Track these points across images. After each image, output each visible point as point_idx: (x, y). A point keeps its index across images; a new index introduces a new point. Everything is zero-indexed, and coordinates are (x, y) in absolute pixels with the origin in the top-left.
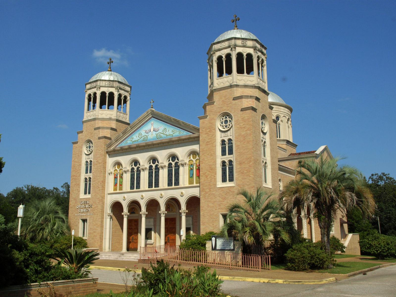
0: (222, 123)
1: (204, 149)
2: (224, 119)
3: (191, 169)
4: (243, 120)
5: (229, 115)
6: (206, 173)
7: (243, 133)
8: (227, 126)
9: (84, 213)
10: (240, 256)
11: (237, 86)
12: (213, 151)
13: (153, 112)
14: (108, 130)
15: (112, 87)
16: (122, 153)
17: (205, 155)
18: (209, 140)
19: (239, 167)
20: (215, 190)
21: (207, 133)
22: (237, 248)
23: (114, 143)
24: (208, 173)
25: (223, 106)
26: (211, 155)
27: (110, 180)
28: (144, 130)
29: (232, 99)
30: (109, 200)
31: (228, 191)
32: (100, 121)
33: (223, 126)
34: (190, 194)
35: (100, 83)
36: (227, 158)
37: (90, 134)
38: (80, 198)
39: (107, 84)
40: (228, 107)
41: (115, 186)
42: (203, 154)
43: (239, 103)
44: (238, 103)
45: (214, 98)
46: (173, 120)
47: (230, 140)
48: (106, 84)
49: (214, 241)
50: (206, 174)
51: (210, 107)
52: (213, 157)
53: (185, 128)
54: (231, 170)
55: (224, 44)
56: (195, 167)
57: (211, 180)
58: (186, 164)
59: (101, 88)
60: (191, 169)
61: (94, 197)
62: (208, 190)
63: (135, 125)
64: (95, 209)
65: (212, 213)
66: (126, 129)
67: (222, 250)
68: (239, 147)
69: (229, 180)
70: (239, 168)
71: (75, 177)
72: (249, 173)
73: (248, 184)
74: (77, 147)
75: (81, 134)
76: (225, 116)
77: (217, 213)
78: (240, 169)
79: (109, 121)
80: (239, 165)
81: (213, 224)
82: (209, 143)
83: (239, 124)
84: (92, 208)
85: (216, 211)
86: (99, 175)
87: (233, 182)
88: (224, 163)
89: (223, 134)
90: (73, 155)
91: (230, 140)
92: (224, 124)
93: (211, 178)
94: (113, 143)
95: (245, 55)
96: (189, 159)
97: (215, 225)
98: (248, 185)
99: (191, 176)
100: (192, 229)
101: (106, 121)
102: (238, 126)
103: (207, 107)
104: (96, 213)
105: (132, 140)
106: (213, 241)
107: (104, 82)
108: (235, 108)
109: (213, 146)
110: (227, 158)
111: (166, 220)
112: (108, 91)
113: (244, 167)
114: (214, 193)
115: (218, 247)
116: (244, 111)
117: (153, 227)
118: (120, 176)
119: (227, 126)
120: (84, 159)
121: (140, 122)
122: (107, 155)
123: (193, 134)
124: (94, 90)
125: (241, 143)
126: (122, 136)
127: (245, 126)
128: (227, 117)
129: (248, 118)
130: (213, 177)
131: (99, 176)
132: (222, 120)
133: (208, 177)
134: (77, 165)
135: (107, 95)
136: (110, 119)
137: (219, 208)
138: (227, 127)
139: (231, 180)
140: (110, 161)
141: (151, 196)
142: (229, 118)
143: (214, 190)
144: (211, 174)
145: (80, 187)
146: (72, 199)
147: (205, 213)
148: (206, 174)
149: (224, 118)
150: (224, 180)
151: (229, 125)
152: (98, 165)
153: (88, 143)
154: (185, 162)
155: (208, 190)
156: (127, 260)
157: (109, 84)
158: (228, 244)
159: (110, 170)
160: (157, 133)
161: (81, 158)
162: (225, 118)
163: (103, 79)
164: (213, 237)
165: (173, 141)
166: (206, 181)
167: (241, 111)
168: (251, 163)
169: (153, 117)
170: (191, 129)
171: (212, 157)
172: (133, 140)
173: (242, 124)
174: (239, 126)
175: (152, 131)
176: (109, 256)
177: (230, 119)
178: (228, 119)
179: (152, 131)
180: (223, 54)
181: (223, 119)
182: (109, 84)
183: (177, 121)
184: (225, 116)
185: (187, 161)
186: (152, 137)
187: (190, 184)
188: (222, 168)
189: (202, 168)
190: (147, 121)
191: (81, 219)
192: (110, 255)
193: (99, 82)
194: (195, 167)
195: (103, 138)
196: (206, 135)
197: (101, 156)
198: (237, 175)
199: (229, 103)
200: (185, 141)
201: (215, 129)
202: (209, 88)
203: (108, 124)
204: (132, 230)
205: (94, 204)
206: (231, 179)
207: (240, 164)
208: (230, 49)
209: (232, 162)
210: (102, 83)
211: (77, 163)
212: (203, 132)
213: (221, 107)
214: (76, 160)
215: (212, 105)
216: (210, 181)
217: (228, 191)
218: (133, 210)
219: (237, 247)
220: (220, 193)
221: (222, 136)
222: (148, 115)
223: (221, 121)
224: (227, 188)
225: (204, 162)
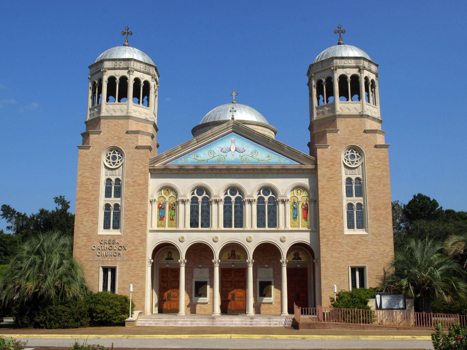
0: (109, 158)
1: (324, 186)
2: (111, 155)
3: (294, 208)
4: (377, 158)
5: (118, 150)
6: (327, 215)
7: (378, 174)
8: (354, 162)
9: (108, 257)
10: (412, 315)
11: (368, 116)
12: (338, 189)
13: (239, 125)
14: (149, 137)
15: (148, 74)
16: (178, 173)
17: (326, 193)
18: (332, 176)
19: (374, 213)
20: (342, 237)
21: (328, 167)
22: (409, 306)
23: (165, 158)
24: (331, 216)
25: (350, 137)
26: (335, 195)
27: (153, 212)
28: (218, 148)
29: (363, 131)
30: (152, 241)
31: (360, 240)
32: (134, 122)
33: (109, 162)
34: (194, 239)
35: (134, 64)
36: (113, 201)
37: (116, 138)
38: (99, 234)
39: (142, 67)
40: (357, 139)
41: (160, 220)
42: (323, 192)
43: (372, 138)
44: (370, 137)
45: (338, 126)
46: (273, 141)
47: (118, 180)
48: (141, 68)
49: (379, 299)
50: (329, 217)
51: (332, 135)
52: (337, 197)
53: (289, 156)
54: (117, 216)
55: (350, 62)
56: (300, 206)
57: (336, 225)
58: (155, 201)
59: (135, 72)
60: (294, 208)
61: (130, 234)
62: (331, 237)
63: (207, 138)
64: (132, 252)
65: (338, 265)
66: (190, 142)
67: (390, 309)
68: (373, 189)
69: (113, 226)
70: (373, 214)
71: (84, 201)
72: (387, 221)
73: (385, 233)
74: (89, 154)
75: (96, 136)
76: (351, 150)
77: (345, 265)
78: (375, 216)
79: (144, 123)
80: (373, 211)
81: (340, 278)
82: (331, 179)
83: (373, 163)
84: (125, 251)
85: (343, 263)
86: (139, 202)
87: (119, 230)
88: (107, 206)
89: (109, 172)
90: (79, 166)
91: (118, 180)
92: (111, 160)
93: (336, 223)
94: (163, 158)
95: (142, 81)
96: (159, 194)
97: (342, 279)
98: (385, 234)
99: (161, 218)
100: (273, 283)
101: (142, 123)
102: (371, 165)
103: (328, 134)
104: (135, 259)
105: (197, 158)
106: (377, 299)
107: (139, 64)
108: (366, 142)
109: (338, 183)
110: (113, 201)
111: (222, 271)
112: (348, 74)
113: (380, 213)
114: (339, 240)
115: (384, 306)
116: (379, 149)
117: (208, 280)
118: (170, 207)
119: (354, 162)
120: (104, 175)
121: (213, 135)
122: (150, 174)
123: (301, 164)
124: (124, 73)
125: (376, 185)
126: (180, 150)
127: (380, 166)
128: (116, 151)
129: (384, 157)
130: (338, 221)
131: (139, 204)
132: (109, 155)
133: (330, 221)
134: (89, 183)
135: (349, 79)
136: (147, 121)
137: (348, 259)
138: (354, 164)
139: (117, 226)
140: (154, 184)
141: (198, 239)
142: (119, 154)
143: (339, 237)
144: (335, 217)
145: (98, 218)
146: (81, 235)
147: (327, 265)
148: (329, 217)
149: (112, 152)
150: (106, 226)
151: (118, 162)
152: (137, 187)
153: (111, 151)
154: (155, 198)
155: (331, 237)
156: (240, 326)
157: (145, 68)
158: (395, 303)
159: (153, 197)
160: (242, 154)
161: (99, 173)
162: (113, 153)
163: (344, 55)
164: (377, 294)
165: (287, 170)
166: (328, 226)
167: (374, 147)
168: (388, 210)
169: (233, 131)
170: (299, 158)
171: (336, 197)
172: (199, 158)
173: (376, 163)
174: (373, 165)
175: (233, 149)
176: (176, 321)
177: (120, 155)
178: (117, 155)
179: (233, 149)
180: (348, 74)
181: (110, 154)
182: (145, 68)
183: (279, 144)
184: (351, 150)
185: (289, 197)
186: (233, 159)
187: (258, 226)
188: (105, 212)
189: (322, 210)
190: (223, 136)
191: (102, 267)
192: (186, 320)
193: (132, 62)
194: (300, 206)
195: (147, 148)
196: (327, 169)
197: (142, 174)
198: (371, 222)
199: (358, 135)
200: (289, 172)
201: (339, 164)
202: (89, 111)
203: (144, 128)
204: (168, 284)
205: (129, 245)
206: (107, 226)
207: (375, 209)
208: (127, 71)
209: (119, 206)
210: (137, 64)
211: (90, 180)
212: (322, 164)
213: (348, 138)
214: (87, 174)
215: (335, 133)
216: (334, 226)
217: (360, 240)
218: (170, 255)
219: (408, 305)
220: (348, 241)
221: (108, 174)
222: (227, 128)
223: (107, 155)
224: (358, 236)
225: (325, 201)
